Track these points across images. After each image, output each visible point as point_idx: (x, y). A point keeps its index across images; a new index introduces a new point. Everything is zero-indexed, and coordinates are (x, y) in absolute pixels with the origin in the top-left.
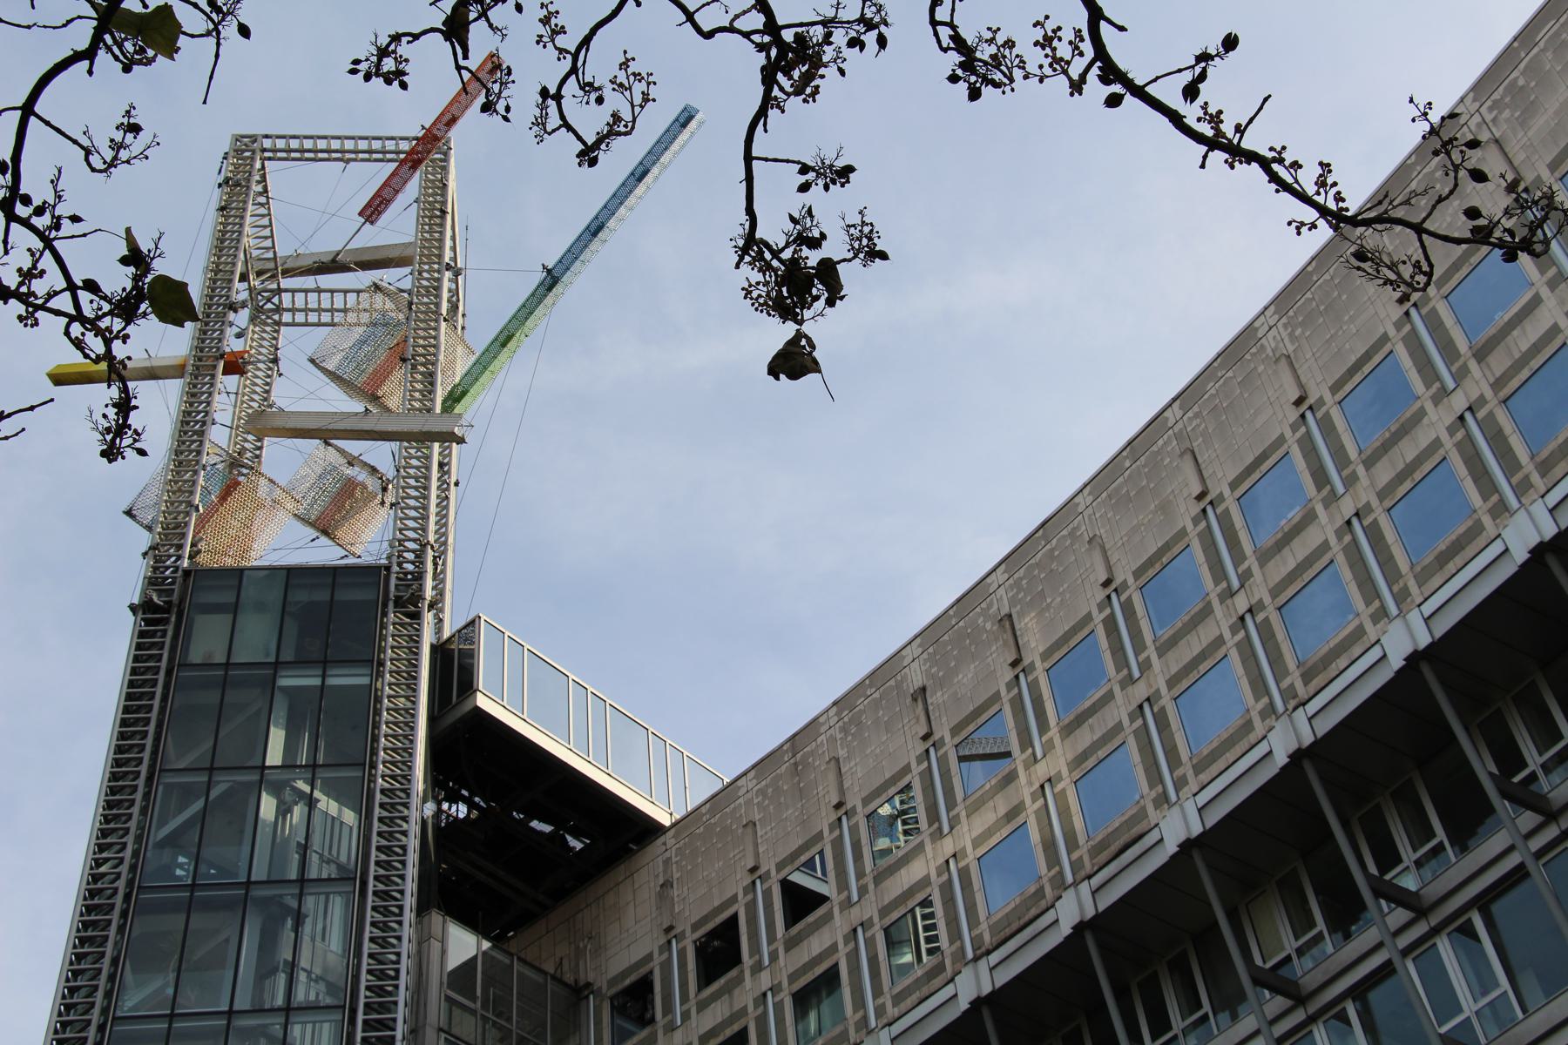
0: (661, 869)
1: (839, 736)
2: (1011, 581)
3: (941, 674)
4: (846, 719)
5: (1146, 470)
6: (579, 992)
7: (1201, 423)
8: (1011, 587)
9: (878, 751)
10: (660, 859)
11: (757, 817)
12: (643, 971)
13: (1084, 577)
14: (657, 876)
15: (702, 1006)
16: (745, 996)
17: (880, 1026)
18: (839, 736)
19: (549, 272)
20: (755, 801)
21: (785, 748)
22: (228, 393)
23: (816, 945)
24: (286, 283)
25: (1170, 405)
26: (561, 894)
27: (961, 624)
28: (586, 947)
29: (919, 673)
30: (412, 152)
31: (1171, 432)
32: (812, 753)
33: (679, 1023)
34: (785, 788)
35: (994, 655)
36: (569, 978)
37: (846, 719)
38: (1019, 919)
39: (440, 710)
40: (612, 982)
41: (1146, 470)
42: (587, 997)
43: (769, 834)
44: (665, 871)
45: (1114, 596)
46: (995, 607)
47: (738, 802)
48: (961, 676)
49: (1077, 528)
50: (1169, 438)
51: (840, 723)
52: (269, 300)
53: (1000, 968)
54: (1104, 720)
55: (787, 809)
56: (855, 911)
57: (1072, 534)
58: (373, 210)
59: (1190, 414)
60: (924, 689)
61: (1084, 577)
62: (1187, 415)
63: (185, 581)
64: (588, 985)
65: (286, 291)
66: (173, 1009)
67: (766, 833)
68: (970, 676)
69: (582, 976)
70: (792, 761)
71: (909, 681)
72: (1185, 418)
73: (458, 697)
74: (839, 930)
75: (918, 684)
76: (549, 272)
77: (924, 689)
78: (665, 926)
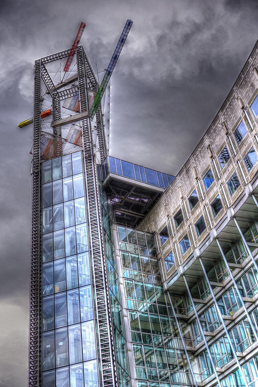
0: (164, 202)
1: (194, 162)
2: (223, 113)
3: (212, 140)
4: (195, 157)
5: (247, 76)
6: (153, 234)
7: (256, 60)
8: (223, 115)
9: (202, 163)
10: (164, 200)
11: (181, 185)
12: (165, 226)
13: (238, 108)
14: (164, 204)
15: (178, 231)
16: (186, 228)
17: (213, 228)
18: (194, 162)
19: (107, 70)
20: (180, 181)
21: (184, 167)
22: (43, 120)
23: (198, 212)
24: (58, 91)
25: (249, 58)
26: (146, 213)
27: (214, 127)
28: (152, 224)
29: (208, 142)
30: (71, 52)
31: (250, 65)
32: (189, 167)
33: (174, 236)
34: (185, 177)
35: (222, 133)
36: (151, 231)
37: (195, 157)
38: (237, 195)
39: (103, 179)
40: (159, 230)
41: (247, 76)
42: (155, 235)
43: (184, 188)
44: (165, 203)
45: (245, 110)
46: (221, 121)
47: (177, 183)
48: (216, 140)
49: (234, 96)
50: (250, 66)
51: (194, 159)
52: (56, 96)
53: (235, 208)
54: (248, 142)
55: (187, 182)
56: (204, 202)
57: (234, 98)
58: (66, 69)
59: (254, 59)
60: (209, 145)
61: (238, 108)
62: (253, 59)
63: (41, 165)
64: (155, 232)
65: (59, 92)
66: (54, 259)
67: (183, 188)
68: (218, 139)
69: (153, 230)
70: (186, 170)
71: (206, 144)
72: (253, 60)
73: (106, 175)
74: (201, 207)
75: (208, 144)
76: (107, 70)
77: (209, 145)
78: (167, 215)
